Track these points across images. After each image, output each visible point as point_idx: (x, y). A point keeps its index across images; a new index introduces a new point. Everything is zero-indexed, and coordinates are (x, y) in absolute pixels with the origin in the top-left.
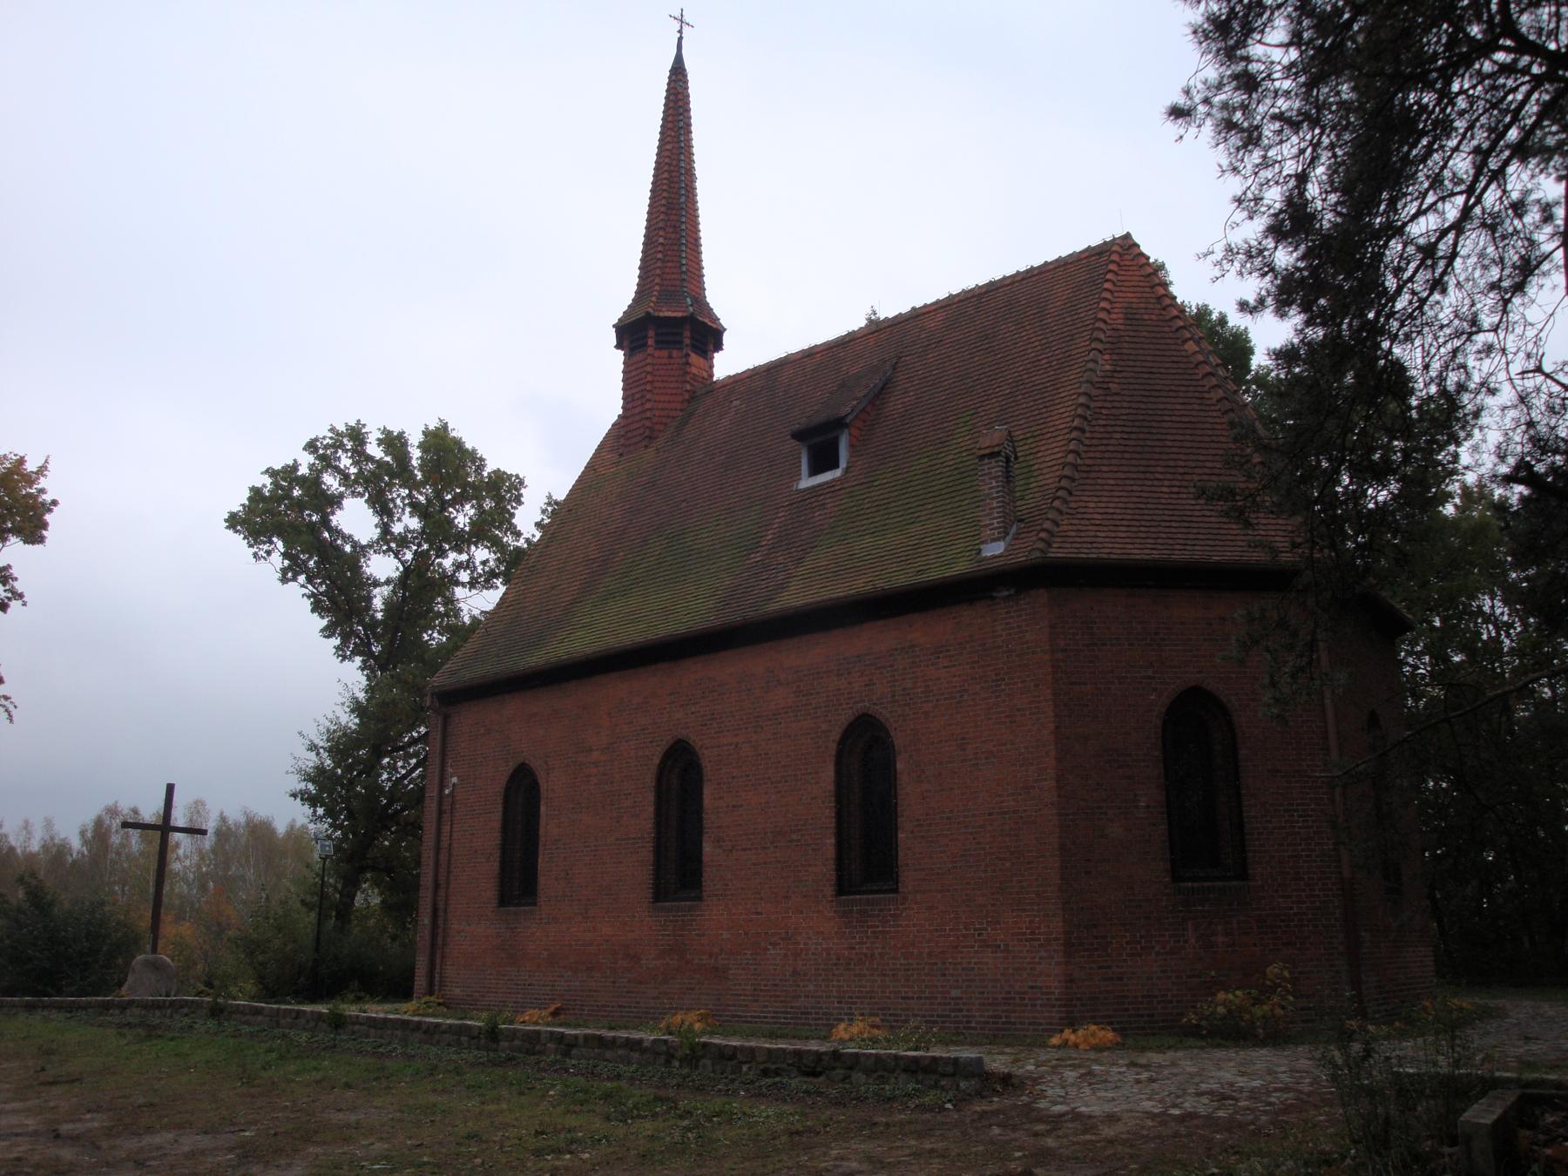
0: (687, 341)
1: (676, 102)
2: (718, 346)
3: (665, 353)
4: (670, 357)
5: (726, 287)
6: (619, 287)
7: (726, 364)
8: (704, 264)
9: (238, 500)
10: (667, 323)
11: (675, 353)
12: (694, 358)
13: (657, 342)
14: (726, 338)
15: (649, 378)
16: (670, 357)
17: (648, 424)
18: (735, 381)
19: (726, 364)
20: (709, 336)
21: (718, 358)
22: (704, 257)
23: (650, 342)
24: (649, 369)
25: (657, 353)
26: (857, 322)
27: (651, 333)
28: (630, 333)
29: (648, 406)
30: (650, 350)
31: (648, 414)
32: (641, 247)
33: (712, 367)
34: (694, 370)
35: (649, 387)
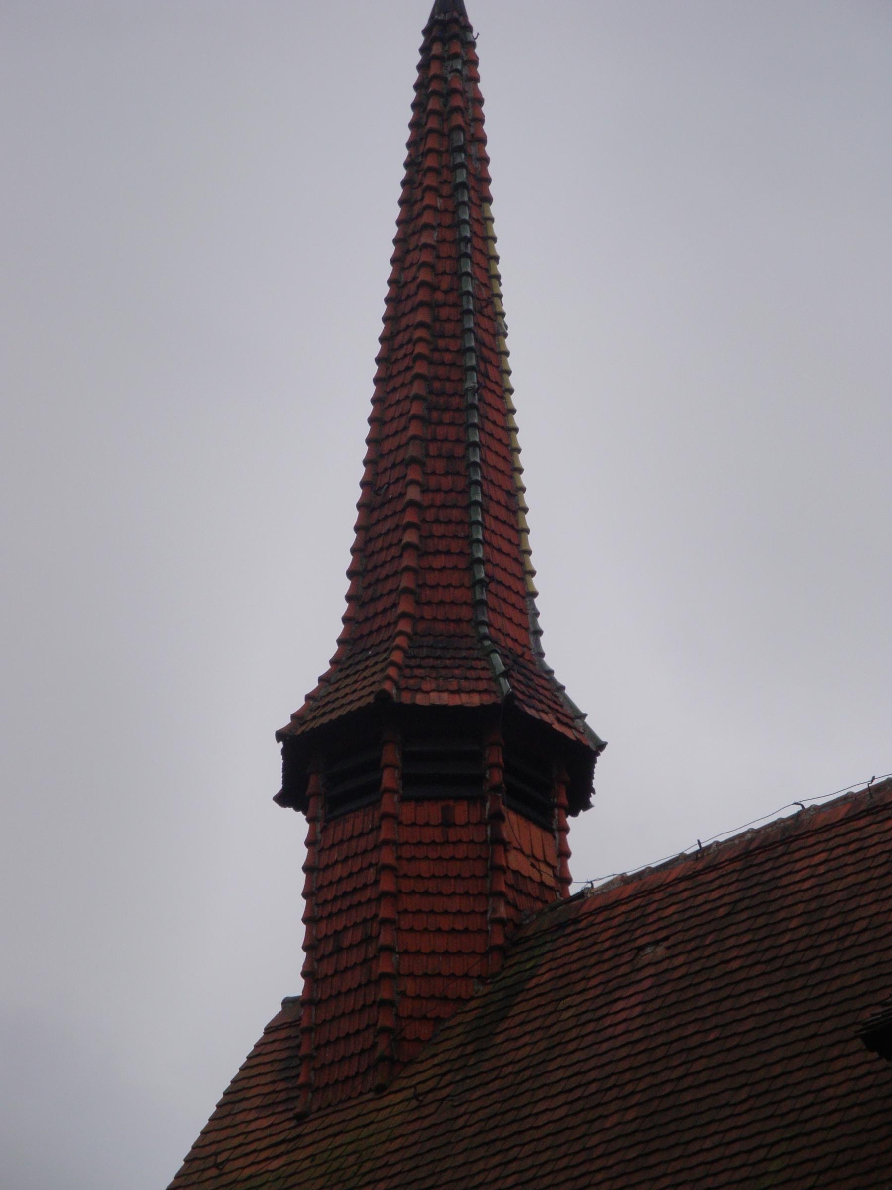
0: (496, 777)
1: (443, 116)
2: (580, 797)
3: (432, 812)
4: (447, 823)
5: (592, 631)
6: (285, 618)
7: (609, 843)
8: (535, 561)
9: (607, 746)
10: (432, 727)
11: (461, 812)
12: (515, 827)
13: (407, 780)
14: (603, 771)
15: (387, 884)
16: (447, 823)
17: (385, 1020)
18: (647, 894)
19: (609, 843)
20: (555, 761)
21: (580, 829)
22: (533, 541)
23: (389, 779)
24: (387, 856)
25: (407, 812)
26: (596, 784)
27: (391, 754)
28: (322, 760)
29: (384, 966)
30: (388, 804)
31: (384, 993)
32: (353, 516)
33: (565, 854)
34: (516, 861)
35: (385, 911)
